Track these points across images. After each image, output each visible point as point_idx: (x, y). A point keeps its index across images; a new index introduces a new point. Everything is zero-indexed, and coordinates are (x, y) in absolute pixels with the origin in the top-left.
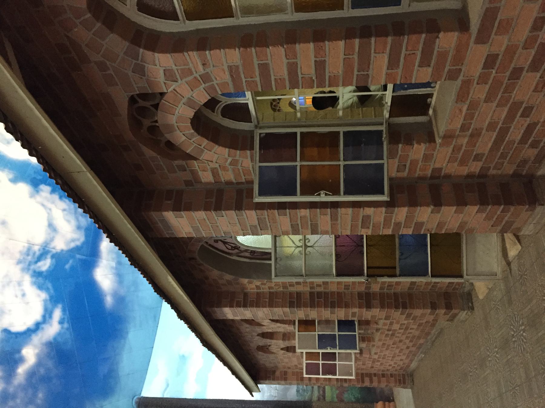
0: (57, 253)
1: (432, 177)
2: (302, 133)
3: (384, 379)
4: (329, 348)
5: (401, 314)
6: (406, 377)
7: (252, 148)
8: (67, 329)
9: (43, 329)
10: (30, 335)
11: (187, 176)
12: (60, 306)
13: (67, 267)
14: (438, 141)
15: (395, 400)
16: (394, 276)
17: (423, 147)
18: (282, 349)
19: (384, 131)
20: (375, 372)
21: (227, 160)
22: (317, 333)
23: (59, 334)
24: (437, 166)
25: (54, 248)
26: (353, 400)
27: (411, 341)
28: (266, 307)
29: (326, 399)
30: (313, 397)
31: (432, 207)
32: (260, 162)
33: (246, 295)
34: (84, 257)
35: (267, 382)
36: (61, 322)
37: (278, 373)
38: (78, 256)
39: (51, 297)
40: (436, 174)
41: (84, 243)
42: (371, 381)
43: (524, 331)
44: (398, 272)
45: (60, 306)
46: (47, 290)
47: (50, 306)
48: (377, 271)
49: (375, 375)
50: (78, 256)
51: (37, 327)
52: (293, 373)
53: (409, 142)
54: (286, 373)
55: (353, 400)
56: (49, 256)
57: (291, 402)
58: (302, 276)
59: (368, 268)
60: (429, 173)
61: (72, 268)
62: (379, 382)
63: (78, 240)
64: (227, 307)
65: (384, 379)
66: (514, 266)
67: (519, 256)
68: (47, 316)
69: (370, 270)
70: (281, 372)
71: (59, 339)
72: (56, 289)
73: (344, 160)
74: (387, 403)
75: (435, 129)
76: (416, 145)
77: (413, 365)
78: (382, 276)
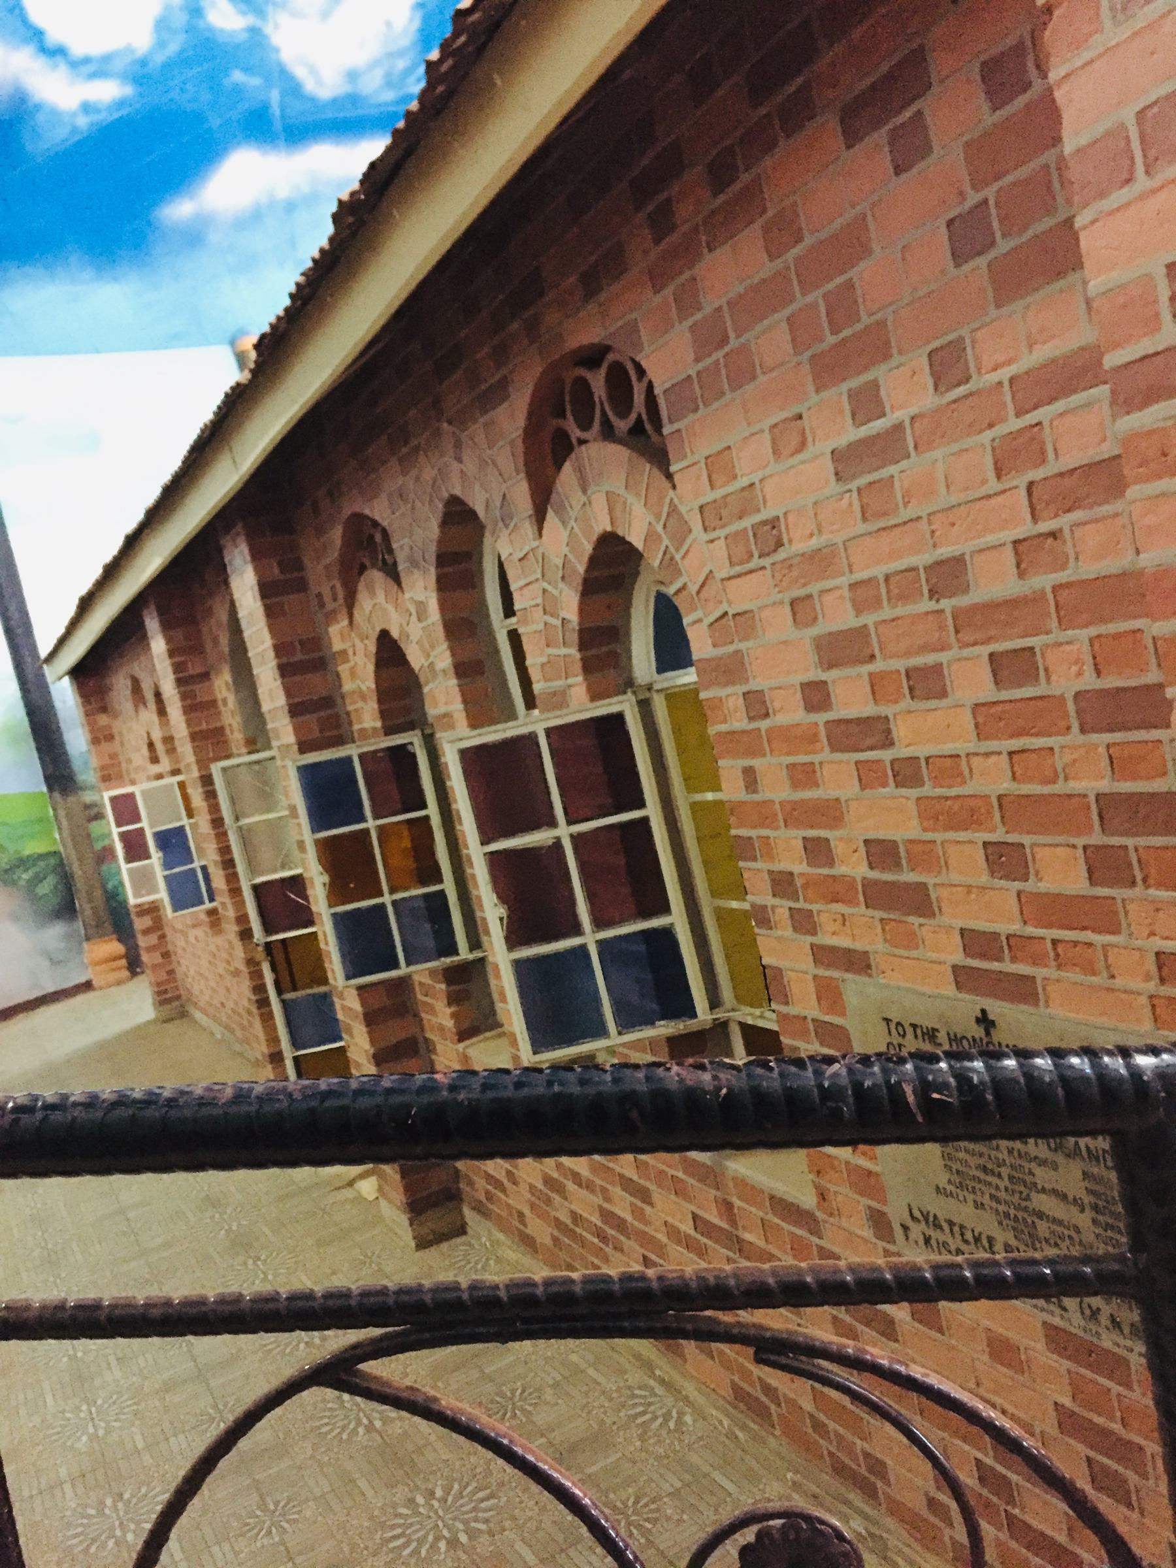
0: (265, 37)
1: (426, 1040)
2: (427, 818)
3: (160, 960)
4: (160, 854)
5: (249, 1000)
6: (176, 1003)
7: (389, 731)
8: (75, 130)
9: (55, 67)
10: (26, 41)
11: (330, 606)
12: (128, 90)
13: (238, 76)
14: (461, 1046)
15: (135, 980)
16: (280, 991)
17: (449, 1023)
18: (148, 733)
19: (456, 958)
20: (169, 937)
21: (363, 682)
22: (564, 832)
23: (54, 112)
24: (439, 1048)
25: (276, 26)
26: (110, 886)
27: (233, 1011)
28: (189, 726)
29: (95, 824)
30: (90, 793)
31: (372, 1051)
32: (361, 756)
33: (205, 676)
34: (276, 110)
35: (79, 700)
36: (86, 108)
37: (103, 720)
38: (275, 96)
39: (143, 62)
40: (430, 1047)
41: (312, 99)
42: (146, 932)
43: (229, 1231)
44: (289, 996)
45: (128, 90)
46: (161, 44)
47: (119, 65)
48: (280, 956)
49: (163, 937)
50: (275, 96)
51: (56, 53)
52: (113, 756)
53: (453, 999)
54: (110, 738)
55: (110, 886)
56: (250, 20)
57: (62, 744)
58: (237, 819)
59: (284, 941)
60: (429, 1035)
61: (238, 90)
62: (150, 949)
63: (319, 82)
64: (167, 643)
65: (157, 958)
66: (348, 1193)
67: (359, 1199)
68: (90, 68)
69: (279, 945)
70: (109, 727)
71: (41, 118)
72: (167, 66)
73: (394, 903)
74: (124, 962)
75: (481, 1037)
76: (449, 1011)
77: (198, 1015)
78: (274, 968)
